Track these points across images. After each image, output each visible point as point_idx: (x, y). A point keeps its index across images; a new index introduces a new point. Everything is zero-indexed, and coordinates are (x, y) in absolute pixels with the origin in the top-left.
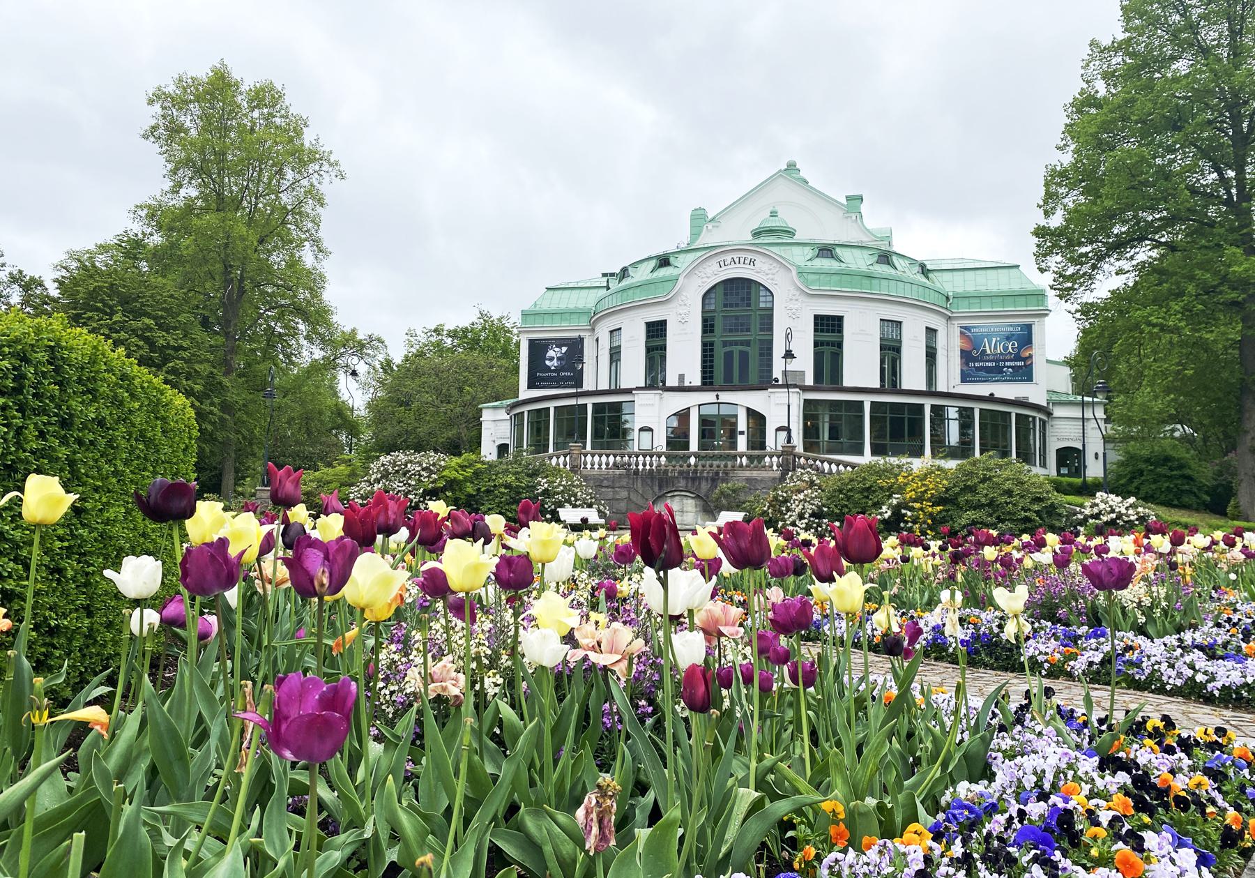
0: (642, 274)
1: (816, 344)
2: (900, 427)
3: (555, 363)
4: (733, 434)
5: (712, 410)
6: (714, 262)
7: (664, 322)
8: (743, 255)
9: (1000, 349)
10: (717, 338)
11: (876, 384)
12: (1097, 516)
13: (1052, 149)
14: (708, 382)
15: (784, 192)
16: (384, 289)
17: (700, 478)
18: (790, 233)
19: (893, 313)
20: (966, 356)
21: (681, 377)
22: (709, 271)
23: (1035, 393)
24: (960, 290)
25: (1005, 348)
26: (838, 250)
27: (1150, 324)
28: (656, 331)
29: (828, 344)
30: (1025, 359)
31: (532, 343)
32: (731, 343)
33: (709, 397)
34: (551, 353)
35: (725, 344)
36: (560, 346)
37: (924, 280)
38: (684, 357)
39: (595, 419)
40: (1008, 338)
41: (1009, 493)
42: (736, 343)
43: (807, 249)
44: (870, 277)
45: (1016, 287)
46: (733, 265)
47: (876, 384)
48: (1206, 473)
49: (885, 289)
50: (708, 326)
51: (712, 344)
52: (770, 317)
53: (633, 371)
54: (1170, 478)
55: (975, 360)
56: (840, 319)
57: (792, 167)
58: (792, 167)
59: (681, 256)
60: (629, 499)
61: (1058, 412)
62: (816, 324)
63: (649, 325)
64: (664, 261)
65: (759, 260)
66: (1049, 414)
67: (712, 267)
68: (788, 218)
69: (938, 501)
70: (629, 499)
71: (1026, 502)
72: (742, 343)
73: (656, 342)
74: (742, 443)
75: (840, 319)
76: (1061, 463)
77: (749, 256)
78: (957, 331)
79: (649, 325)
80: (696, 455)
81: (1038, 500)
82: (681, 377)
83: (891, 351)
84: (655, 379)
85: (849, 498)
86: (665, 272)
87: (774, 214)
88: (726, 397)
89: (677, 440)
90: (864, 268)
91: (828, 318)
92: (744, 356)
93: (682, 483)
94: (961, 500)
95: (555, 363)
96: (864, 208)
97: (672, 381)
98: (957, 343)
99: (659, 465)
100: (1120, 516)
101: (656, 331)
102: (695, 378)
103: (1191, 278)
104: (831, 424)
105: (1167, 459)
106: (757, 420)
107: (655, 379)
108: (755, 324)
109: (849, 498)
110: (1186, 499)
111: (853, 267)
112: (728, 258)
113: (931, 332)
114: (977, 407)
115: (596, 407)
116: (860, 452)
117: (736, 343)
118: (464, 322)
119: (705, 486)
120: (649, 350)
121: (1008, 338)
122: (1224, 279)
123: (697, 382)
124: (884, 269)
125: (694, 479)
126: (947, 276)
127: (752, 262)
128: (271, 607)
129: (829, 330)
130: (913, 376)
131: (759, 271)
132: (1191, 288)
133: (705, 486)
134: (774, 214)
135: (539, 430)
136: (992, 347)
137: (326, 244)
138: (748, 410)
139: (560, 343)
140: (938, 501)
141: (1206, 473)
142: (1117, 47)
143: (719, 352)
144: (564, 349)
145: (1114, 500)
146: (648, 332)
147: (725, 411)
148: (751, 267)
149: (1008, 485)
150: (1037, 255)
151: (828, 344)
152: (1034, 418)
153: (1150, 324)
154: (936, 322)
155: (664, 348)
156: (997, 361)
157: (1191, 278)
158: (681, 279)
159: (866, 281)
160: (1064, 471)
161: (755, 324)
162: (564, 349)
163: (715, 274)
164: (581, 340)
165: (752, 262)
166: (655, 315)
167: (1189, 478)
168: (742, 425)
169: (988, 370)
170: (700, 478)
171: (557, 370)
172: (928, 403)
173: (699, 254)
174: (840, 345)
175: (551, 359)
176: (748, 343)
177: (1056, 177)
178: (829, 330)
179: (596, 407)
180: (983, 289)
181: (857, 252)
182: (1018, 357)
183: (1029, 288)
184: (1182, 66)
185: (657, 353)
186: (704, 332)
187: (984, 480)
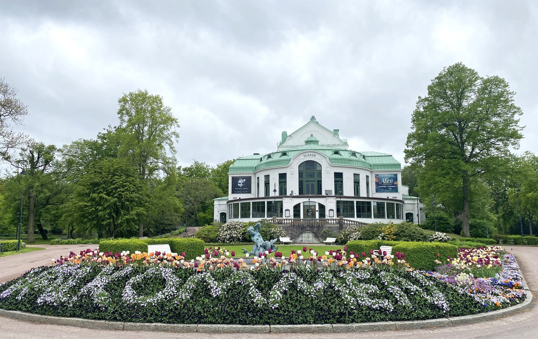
0: (276, 157)
1: (335, 182)
2: (364, 209)
3: (241, 185)
5: (308, 204)
6: (302, 155)
7: (286, 174)
8: (312, 153)
9: (388, 182)
10: (304, 179)
11: (353, 195)
12: (437, 239)
13: (410, 128)
17: (314, 227)
19: (357, 172)
20: (377, 184)
21: (292, 192)
22: (301, 158)
23: (399, 196)
24: (374, 163)
25: (389, 182)
26: (340, 152)
27: (441, 182)
28: (283, 177)
30: (395, 185)
31: (233, 178)
32: (308, 181)
34: (240, 181)
35: (306, 181)
36: (243, 179)
37: (363, 160)
38: (293, 185)
39: (268, 207)
40: (390, 179)
41: (414, 233)
42: (311, 181)
43: (331, 151)
44: (350, 160)
45: (392, 162)
48: (452, 221)
49: (354, 164)
50: (301, 175)
51: (302, 181)
52: (321, 173)
54: (444, 224)
55: (380, 185)
56: (342, 173)
57: (313, 118)
58: (313, 118)
59: (290, 152)
60: (292, 233)
61: (406, 202)
64: (284, 154)
65: (317, 155)
66: (403, 202)
67: (302, 157)
68: (316, 137)
69: (394, 235)
70: (292, 233)
71: (418, 235)
72: (311, 181)
73: (283, 180)
74: (317, 214)
75: (342, 173)
76: (407, 218)
77: (314, 154)
78: (374, 176)
81: (422, 234)
82: (292, 192)
83: (357, 183)
85: (368, 234)
86: (284, 157)
87: (312, 136)
88: (312, 200)
90: (348, 158)
91: (338, 173)
92: (313, 185)
93: (308, 228)
94: (401, 234)
95: (241, 185)
98: (374, 180)
100: (443, 238)
101: (283, 177)
102: (296, 193)
103: (451, 169)
104: (344, 208)
105: (442, 218)
106: (322, 207)
108: (316, 175)
109: (368, 234)
110: (448, 230)
111: (345, 157)
112: (307, 154)
113: (367, 177)
116: (354, 217)
117: (311, 181)
118: (189, 166)
119: (315, 229)
121: (390, 179)
122: (460, 170)
123: (297, 194)
124: (353, 158)
125: (312, 227)
126: (370, 158)
127: (315, 156)
129: (338, 176)
130: (363, 193)
131: (317, 158)
132: (451, 172)
133: (315, 229)
134: (312, 136)
136: (385, 181)
137: (176, 149)
139: (243, 178)
140: (394, 235)
141: (452, 221)
142: (426, 99)
143: (305, 184)
144: (244, 180)
145: (441, 234)
146: (280, 176)
149: (414, 230)
150: (405, 158)
153: (441, 182)
154: (368, 174)
156: (387, 186)
157: (451, 169)
158: (292, 160)
159: (349, 162)
160: (408, 220)
161: (316, 175)
162: (244, 180)
163: (303, 159)
164: (251, 177)
165: (315, 156)
166: (282, 171)
167: (448, 223)
169: (384, 188)
170: (314, 227)
171: (242, 187)
173: (297, 152)
174: (342, 182)
175: (240, 183)
176: (314, 181)
177: (411, 137)
178: (338, 176)
180: (381, 163)
181: (345, 152)
182: (393, 185)
183: (396, 163)
184: (444, 108)
186: (299, 177)
187: (406, 229)
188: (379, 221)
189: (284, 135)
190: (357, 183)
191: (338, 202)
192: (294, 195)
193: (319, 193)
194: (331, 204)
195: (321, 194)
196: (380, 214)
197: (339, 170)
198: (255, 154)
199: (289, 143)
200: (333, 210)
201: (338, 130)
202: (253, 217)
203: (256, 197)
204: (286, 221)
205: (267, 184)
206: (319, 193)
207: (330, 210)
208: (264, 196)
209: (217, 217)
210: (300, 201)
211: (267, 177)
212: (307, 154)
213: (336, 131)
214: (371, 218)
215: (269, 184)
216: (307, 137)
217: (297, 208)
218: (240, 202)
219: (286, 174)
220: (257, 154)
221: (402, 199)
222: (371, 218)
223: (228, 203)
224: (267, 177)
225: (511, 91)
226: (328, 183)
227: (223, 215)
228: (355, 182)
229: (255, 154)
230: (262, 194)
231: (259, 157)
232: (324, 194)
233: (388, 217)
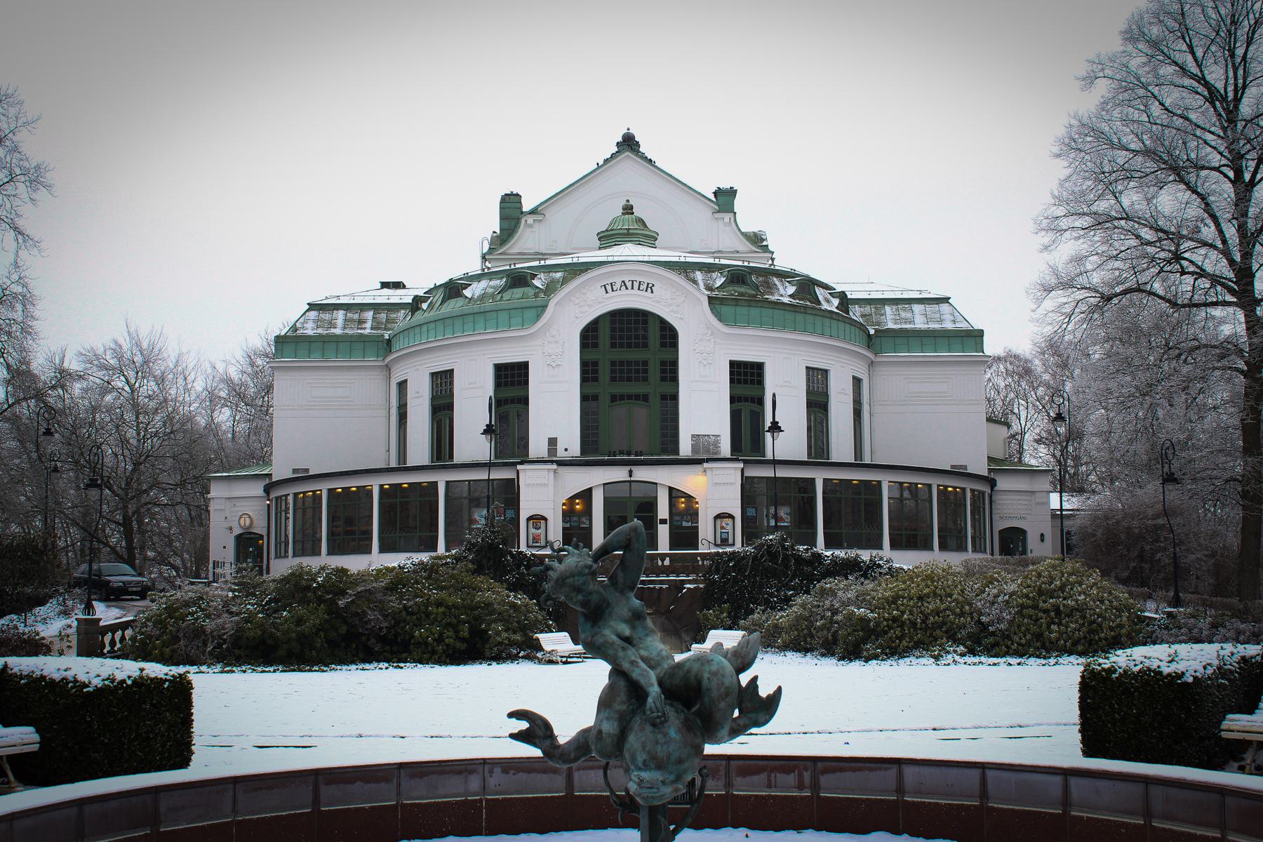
1: (733, 400)
4: (651, 522)
5: (623, 492)
7: (525, 366)
14: (595, 448)
15: (628, 173)
16: (898, 496)
18: (974, 337)
21: (553, 442)
28: (512, 379)
29: (746, 399)
38: (556, 412)
46: (636, 291)
57: (629, 143)
58: (629, 143)
62: (731, 373)
63: (499, 368)
75: (759, 367)
79: (499, 368)
82: (553, 442)
87: (628, 209)
89: (576, 532)
96: (738, 204)
101: (512, 379)
102: (571, 443)
113: (857, 382)
127: (650, 287)
129: (746, 378)
130: (841, 448)
134: (628, 209)
135: (350, 521)
138: (671, 489)
147: (638, 492)
151: (746, 399)
155: (525, 401)
165: (650, 287)
168: (663, 511)
172: (441, 479)
178: (746, 378)
183: (964, 326)
185: (512, 409)
188: (955, 560)
189: (511, 207)
190: (818, 404)
191: (748, 486)
192: (561, 454)
193: (664, 447)
194: (716, 491)
195: (677, 451)
196: (909, 538)
197: (748, 354)
198: (385, 285)
199: (528, 240)
200: (732, 517)
201: (732, 193)
202: (330, 553)
203: (393, 464)
205: (442, 407)
206: (664, 447)
207: (719, 517)
209: (222, 547)
210: (597, 478)
213: (725, 199)
215: (450, 407)
216: (608, 214)
219: (525, 366)
220: (398, 285)
222: (931, 549)
223: (267, 490)
224: (443, 382)
226: (703, 409)
227: (248, 545)
228: (810, 404)
229: (385, 285)
230: (420, 449)
231: (405, 297)
232: (685, 449)
233: (943, 547)
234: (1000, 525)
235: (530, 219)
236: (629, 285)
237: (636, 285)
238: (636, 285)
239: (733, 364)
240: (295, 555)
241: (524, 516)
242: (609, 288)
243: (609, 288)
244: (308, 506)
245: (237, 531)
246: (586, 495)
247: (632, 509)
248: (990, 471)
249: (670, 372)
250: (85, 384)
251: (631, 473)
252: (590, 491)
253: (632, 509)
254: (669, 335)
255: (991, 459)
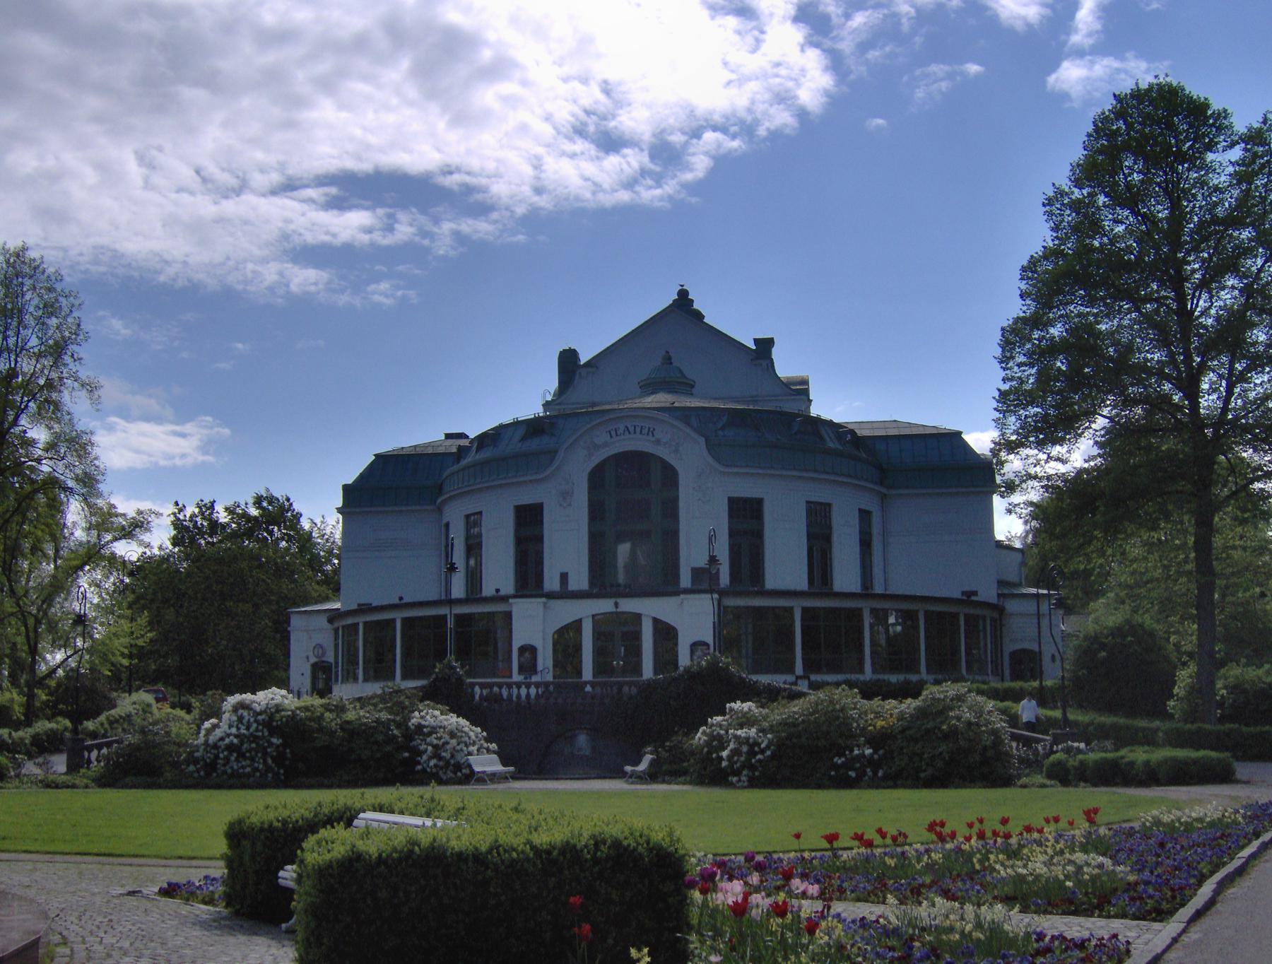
11: (803, 585)
14: (601, 583)
21: (564, 577)
28: (529, 521)
33: (604, 606)
38: (566, 552)
47: (803, 585)
53: (499, 573)
80: (593, 684)
82: (564, 577)
84: (529, 577)
87: (668, 360)
91: (745, 501)
97: (551, 582)
99: (528, 695)
101: (529, 521)
102: (579, 581)
106: (666, 633)
107: (529, 577)
113: (865, 515)
114: (921, 609)
115: (406, 621)
120: (519, 541)
127: (651, 432)
128: (352, 224)
129: (746, 517)
130: (846, 577)
134: (668, 360)
138: (656, 621)
148: (650, 437)
152: (984, 618)
155: (540, 539)
165: (651, 432)
179: (406, 621)
186: (676, 500)
189: (568, 360)
194: (694, 619)
197: (746, 489)
199: (582, 393)
200: (707, 645)
204: (523, 691)
208: (689, 585)
211: (473, 521)
212: (622, 428)
214: (356, 679)
217: (566, 641)
218: (398, 616)
221: (994, 600)
224: (473, 521)
225: (1052, 189)
226: (702, 534)
234: (1009, 647)
235: (584, 372)
236: (631, 429)
237: (638, 430)
238: (638, 430)
239: (731, 500)
240: (365, 680)
241: (516, 645)
242: (613, 433)
243: (613, 433)
244: (380, 633)
245: (313, 660)
246: (577, 625)
247: (618, 636)
248: (999, 596)
249: (671, 510)
250: (32, 530)
251: (616, 605)
252: (580, 620)
253: (618, 636)
254: (670, 476)
255: (1002, 583)
